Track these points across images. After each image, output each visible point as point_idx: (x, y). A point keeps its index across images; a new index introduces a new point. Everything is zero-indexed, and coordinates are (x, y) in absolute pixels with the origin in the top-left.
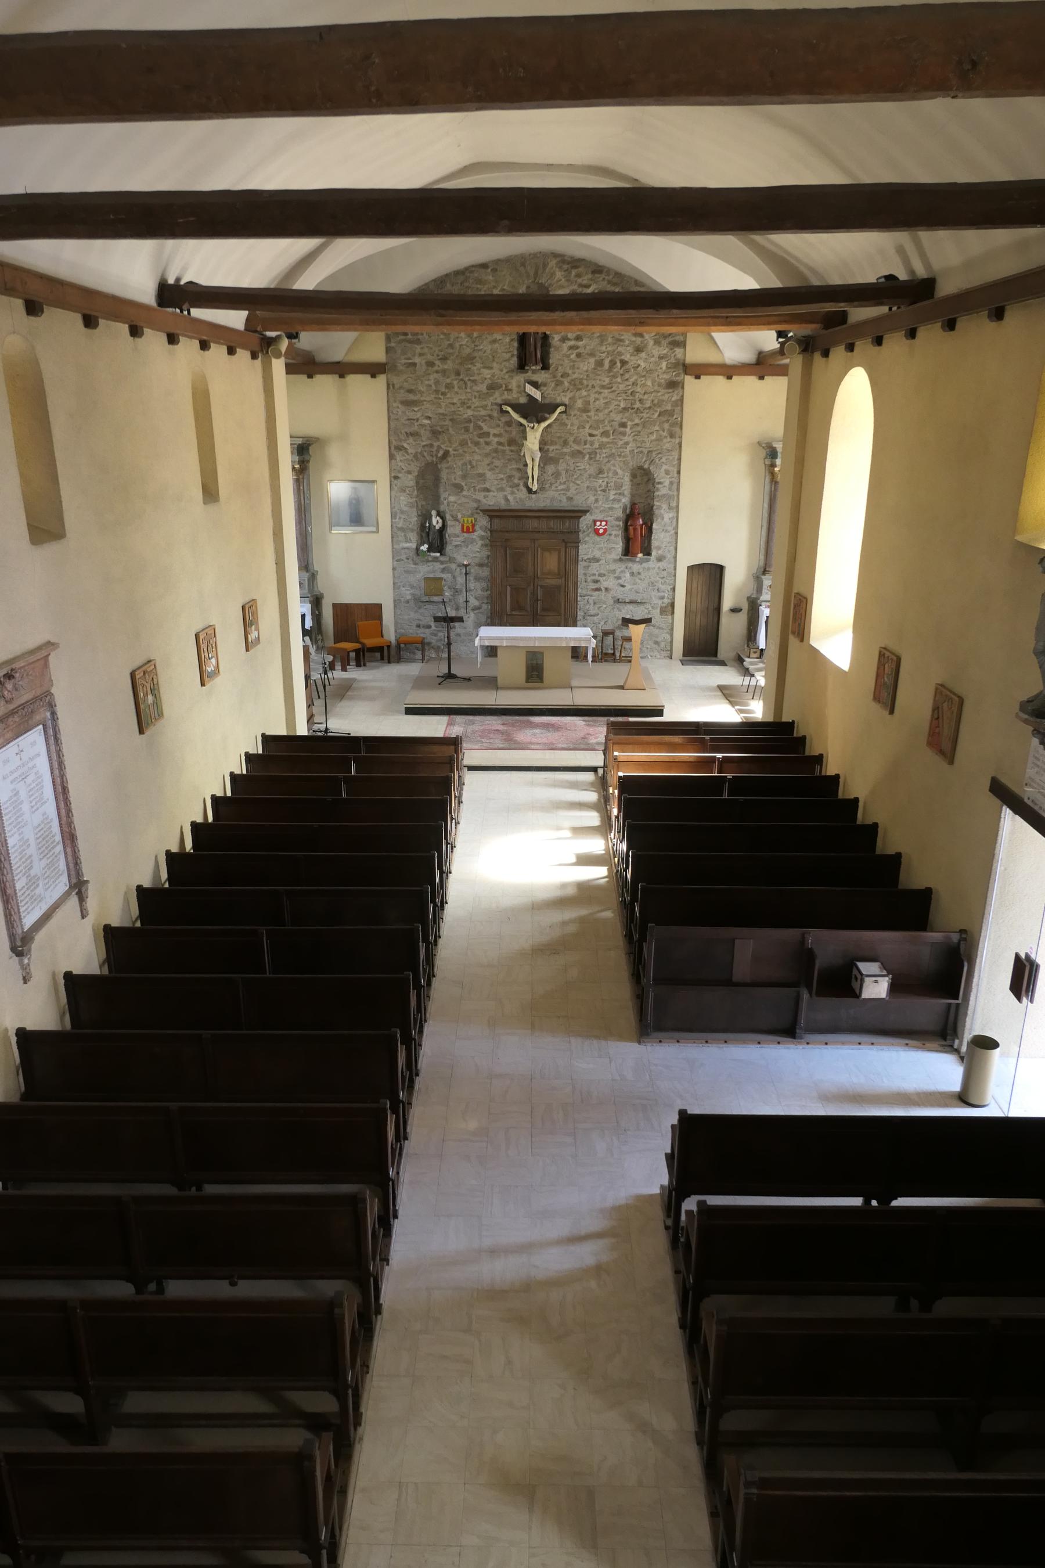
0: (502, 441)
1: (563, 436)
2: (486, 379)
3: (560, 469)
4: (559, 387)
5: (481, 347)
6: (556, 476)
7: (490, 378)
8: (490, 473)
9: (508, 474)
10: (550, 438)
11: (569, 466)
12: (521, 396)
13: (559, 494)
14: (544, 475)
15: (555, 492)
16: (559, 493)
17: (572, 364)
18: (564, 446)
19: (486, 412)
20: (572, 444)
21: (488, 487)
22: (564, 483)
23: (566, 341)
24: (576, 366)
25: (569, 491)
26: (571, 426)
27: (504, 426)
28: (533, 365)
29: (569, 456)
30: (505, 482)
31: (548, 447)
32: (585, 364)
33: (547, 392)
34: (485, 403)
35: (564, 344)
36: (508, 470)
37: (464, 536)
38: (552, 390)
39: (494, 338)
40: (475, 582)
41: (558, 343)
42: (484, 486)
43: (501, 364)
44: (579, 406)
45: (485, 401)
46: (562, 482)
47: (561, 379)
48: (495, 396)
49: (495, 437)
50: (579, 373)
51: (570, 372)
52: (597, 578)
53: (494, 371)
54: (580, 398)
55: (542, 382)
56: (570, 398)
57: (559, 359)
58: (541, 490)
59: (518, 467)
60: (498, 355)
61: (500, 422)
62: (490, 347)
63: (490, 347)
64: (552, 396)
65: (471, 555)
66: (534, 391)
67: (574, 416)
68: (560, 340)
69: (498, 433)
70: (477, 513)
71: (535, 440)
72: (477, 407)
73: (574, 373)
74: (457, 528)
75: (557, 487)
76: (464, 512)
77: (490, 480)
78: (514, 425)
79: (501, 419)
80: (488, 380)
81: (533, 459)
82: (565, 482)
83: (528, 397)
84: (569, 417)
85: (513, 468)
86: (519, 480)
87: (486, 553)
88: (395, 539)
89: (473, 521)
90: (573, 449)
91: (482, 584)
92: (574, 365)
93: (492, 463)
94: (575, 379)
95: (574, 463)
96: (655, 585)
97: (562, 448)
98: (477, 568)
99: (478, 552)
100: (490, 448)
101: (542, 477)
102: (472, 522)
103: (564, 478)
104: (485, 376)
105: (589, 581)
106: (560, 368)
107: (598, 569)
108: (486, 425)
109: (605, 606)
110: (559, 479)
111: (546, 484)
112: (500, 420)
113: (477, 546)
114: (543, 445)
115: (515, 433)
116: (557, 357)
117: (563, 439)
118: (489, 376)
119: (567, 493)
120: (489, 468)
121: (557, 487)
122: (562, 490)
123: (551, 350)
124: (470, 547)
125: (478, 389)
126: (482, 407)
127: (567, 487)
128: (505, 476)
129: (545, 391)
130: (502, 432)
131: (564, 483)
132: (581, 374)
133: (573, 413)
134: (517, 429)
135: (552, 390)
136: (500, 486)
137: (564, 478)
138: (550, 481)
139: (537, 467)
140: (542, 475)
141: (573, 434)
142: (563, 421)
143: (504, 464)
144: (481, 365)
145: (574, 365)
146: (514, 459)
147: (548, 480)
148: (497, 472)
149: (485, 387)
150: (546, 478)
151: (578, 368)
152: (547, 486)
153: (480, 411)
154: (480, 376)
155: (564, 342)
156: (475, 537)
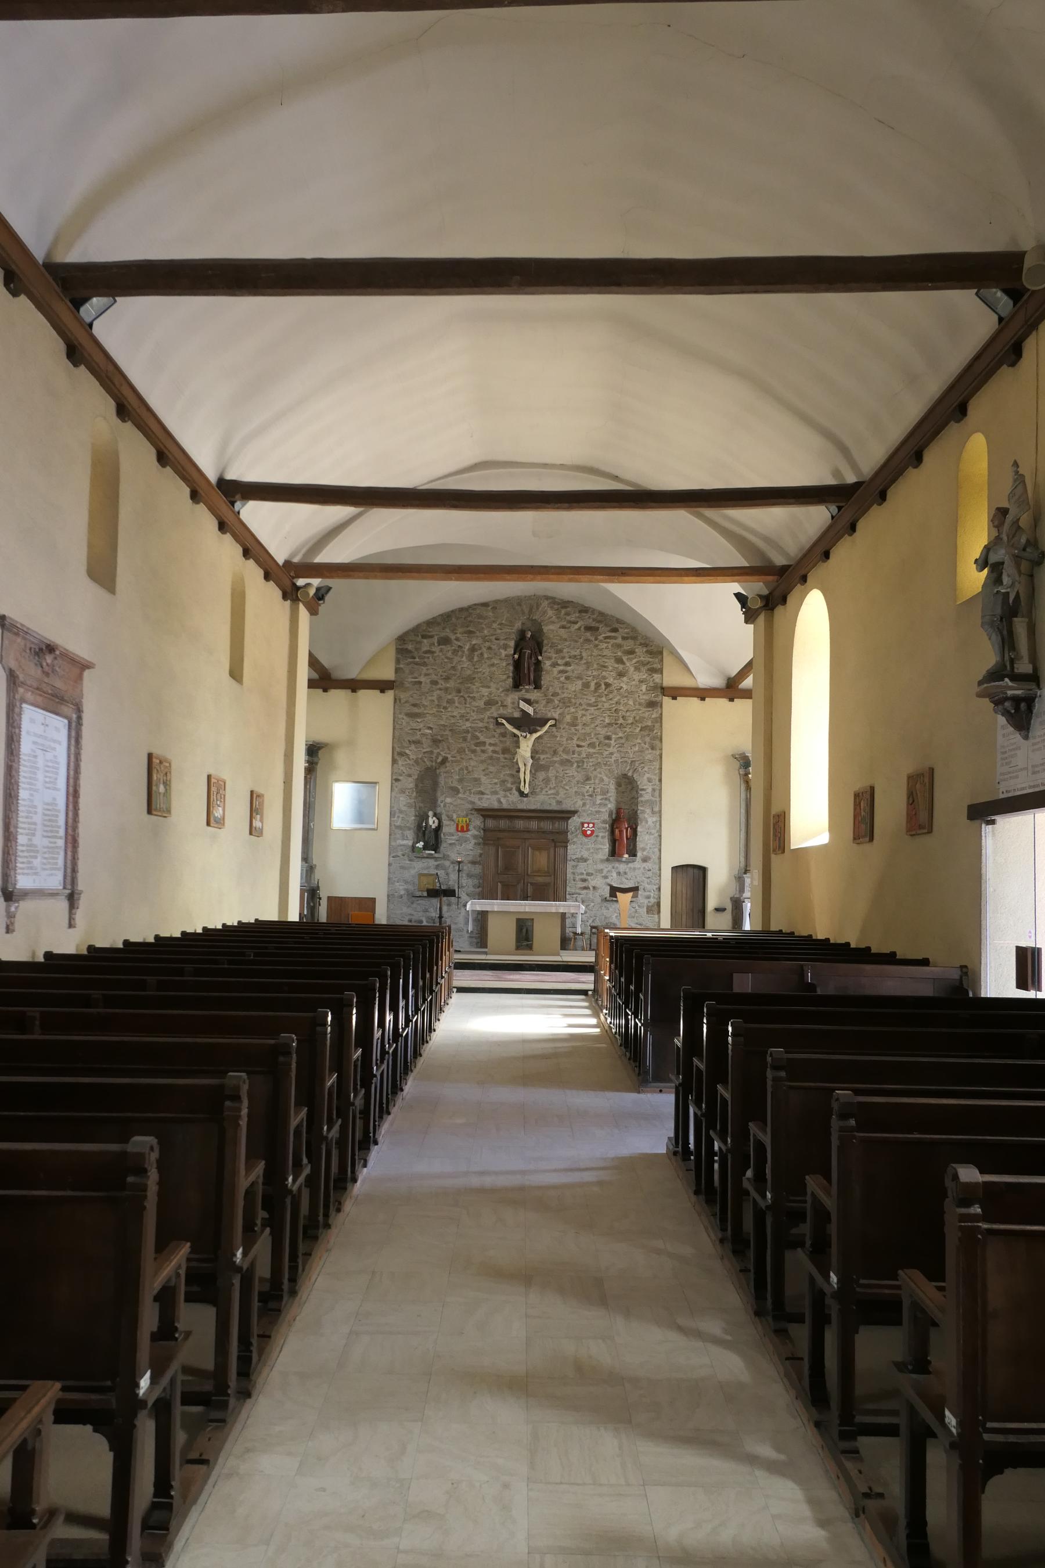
2: (483, 696)
3: (550, 775)
5: (481, 670)
7: (487, 696)
8: (485, 778)
15: (545, 796)
16: (549, 797)
18: (553, 755)
22: (554, 788)
23: (557, 666)
24: (565, 687)
25: (558, 795)
27: (499, 737)
30: (499, 786)
36: (502, 776)
37: (458, 835)
38: (543, 707)
40: (467, 879)
42: (479, 789)
43: (498, 683)
46: (552, 787)
47: (552, 698)
51: (560, 692)
52: (584, 877)
54: (568, 714)
56: (560, 714)
57: (549, 681)
60: (496, 676)
62: (488, 670)
63: (488, 670)
65: (464, 853)
67: (564, 729)
68: (551, 666)
70: (471, 814)
73: (563, 693)
74: (452, 827)
75: (547, 792)
76: (459, 813)
78: (508, 736)
81: (525, 765)
84: (559, 730)
87: (479, 851)
89: (468, 821)
91: (474, 881)
92: (563, 687)
93: (487, 769)
94: (564, 697)
98: (469, 865)
99: (471, 850)
102: (466, 822)
103: (554, 783)
105: (577, 879)
106: (551, 688)
107: (586, 868)
109: (592, 904)
112: (495, 732)
113: (470, 845)
117: (553, 749)
118: (487, 694)
120: (484, 773)
121: (547, 792)
122: (551, 794)
124: (463, 845)
125: (477, 704)
126: (479, 720)
129: (537, 708)
131: (554, 788)
132: (570, 694)
133: (562, 728)
135: (543, 707)
136: (493, 790)
137: (554, 783)
140: (533, 780)
141: (563, 745)
146: (507, 766)
151: (567, 689)
153: (477, 724)
155: (554, 667)
156: (468, 836)
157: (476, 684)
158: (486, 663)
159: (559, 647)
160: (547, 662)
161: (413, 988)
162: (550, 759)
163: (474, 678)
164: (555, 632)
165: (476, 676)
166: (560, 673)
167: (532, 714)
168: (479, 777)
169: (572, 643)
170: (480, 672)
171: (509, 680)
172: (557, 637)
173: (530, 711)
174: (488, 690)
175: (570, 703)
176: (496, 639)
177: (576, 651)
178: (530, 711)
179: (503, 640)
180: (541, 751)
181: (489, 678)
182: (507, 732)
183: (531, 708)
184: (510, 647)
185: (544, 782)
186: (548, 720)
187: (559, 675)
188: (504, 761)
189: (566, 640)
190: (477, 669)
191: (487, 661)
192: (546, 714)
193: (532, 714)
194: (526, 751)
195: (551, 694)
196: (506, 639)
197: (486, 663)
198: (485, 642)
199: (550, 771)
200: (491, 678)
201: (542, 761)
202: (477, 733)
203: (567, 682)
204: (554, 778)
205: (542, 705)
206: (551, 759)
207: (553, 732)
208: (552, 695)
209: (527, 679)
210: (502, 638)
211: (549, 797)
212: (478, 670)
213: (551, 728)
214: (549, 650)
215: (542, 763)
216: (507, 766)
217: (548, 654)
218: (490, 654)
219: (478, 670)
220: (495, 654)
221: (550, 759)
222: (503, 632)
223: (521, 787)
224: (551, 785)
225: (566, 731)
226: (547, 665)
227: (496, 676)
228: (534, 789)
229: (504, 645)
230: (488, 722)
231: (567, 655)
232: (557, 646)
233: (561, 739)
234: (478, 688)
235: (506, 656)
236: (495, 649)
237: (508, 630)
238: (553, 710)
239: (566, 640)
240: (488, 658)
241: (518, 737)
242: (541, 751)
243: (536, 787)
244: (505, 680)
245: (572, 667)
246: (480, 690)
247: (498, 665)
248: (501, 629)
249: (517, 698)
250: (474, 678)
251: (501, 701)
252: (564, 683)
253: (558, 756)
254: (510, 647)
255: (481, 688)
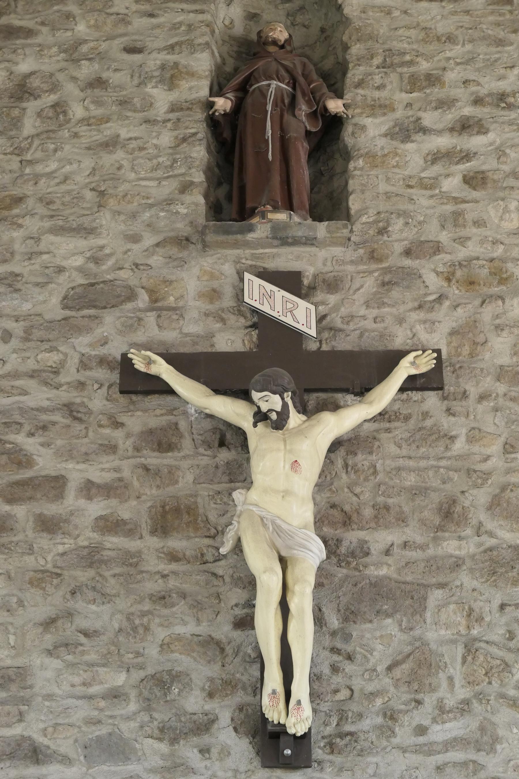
0: (125, 515)
1: (436, 483)
2: (60, 270)
3: (431, 636)
4: (395, 293)
5: (53, 166)
6: (413, 672)
7: (80, 270)
8: (55, 664)
9: (150, 671)
10: (366, 496)
11: (480, 619)
12: (220, 330)
13: (439, 769)
14: (349, 667)
15: (414, 759)
16: (440, 759)
17: (449, 208)
18: (440, 528)
19: (52, 393)
20: (483, 516)
21: (40, 739)
23: (419, 137)
24: (470, 217)
25: (492, 750)
26: (470, 440)
27: (137, 449)
28: (276, 209)
29: (471, 570)
30: (133, 707)
31: (362, 534)
32: (506, 210)
33: (344, 311)
34: (53, 358)
35: (410, 146)
36: (153, 651)
38: (367, 304)
39: (108, 133)
41: (382, 142)
42: (17, 730)
43: (134, 216)
44: (499, 361)
45: (51, 350)
46: (450, 702)
47: (407, 262)
48: (100, 331)
49: (90, 498)
50: (483, 241)
51: (444, 237)
53: (100, 242)
54: (499, 328)
55: (315, 276)
56: (453, 333)
57: (388, 196)
58: (332, 748)
59: (203, 629)
60: (123, 188)
61: (118, 434)
62: (88, 163)
63: (88, 163)
64: (369, 324)
66: (273, 309)
67: (482, 398)
68: (389, 135)
69: (108, 477)
71: (296, 478)
72: (15, 375)
73: (462, 241)
77: (49, 697)
78: (187, 444)
79: (123, 418)
80: (75, 274)
81: (283, 561)
82: (467, 702)
83: (255, 334)
84: (457, 406)
85: (179, 638)
86: (211, 695)
88: (63, 322)
90: (492, 542)
92: (457, 215)
93: (70, 615)
94: (470, 260)
95: (502, 607)
96: (474, 368)
97: (435, 539)
100: (61, 549)
101: (338, 680)
103: (458, 681)
104: (58, 261)
106: (397, 225)
108: (46, 445)
110: (433, 689)
111: (360, 716)
112: (117, 425)
114: (333, 524)
115: (190, 478)
116: (383, 187)
117: (435, 498)
118: (78, 261)
119: (481, 757)
120: (49, 639)
121: (421, 730)
123: (352, 165)
125: (26, 307)
126: (32, 375)
127: (482, 729)
128: (137, 675)
129: (336, 308)
130: (126, 473)
132: (495, 242)
133: (473, 391)
134: (205, 461)
135: (367, 304)
136: (103, 731)
137: (458, 681)
138: (379, 702)
139: (309, 589)
140: (335, 669)
141: (488, 474)
142: (428, 423)
143: (129, 617)
144: (47, 224)
145: (457, 215)
146: (183, 596)
147: (373, 695)
148: (92, 657)
149: (55, 300)
150: (357, 683)
151: (479, 223)
152: (366, 724)
153: (25, 393)
154: (38, 261)
155: (407, 138)
157: (27, 221)
158: (76, 135)
159: (424, 66)
160: (368, 121)
161: (268, 140)
162: (423, 547)
163: (19, 200)
164: (397, 13)
165: (29, 189)
166: (434, 161)
167: (313, 332)
168: (19, 662)
169: (482, 49)
170: (50, 175)
171: (188, 198)
172: (413, 33)
173: (302, 318)
174: (82, 244)
175: (502, 281)
176: (131, 50)
177: (501, 78)
178: (302, 318)
179: (159, 50)
180: (368, 512)
181: (89, 195)
182: (183, 425)
183: (302, 304)
184: (192, 74)
185: (397, 672)
186: (400, 355)
187: (436, 169)
188: (164, 567)
189: (450, 39)
190: (30, 162)
191: (83, 129)
192: (354, 82)
193: (313, 332)
194: (286, 493)
195: (398, 248)
196: (171, 48)
197: (76, 135)
198: (76, 61)
199: (428, 615)
200: (102, 194)
201: (378, 565)
202: (20, 439)
203: (475, 194)
204: (460, 650)
205: (360, 297)
206: (431, 552)
207: (426, 415)
208: (408, 253)
209: (276, 179)
210: (160, 43)
211: (440, 759)
212: (39, 168)
213: (416, 396)
214: (377, 80)
215: (383, 571)
216: (183, 596)
217: (377, 94)
218: (98, 103)
219: (39, 168)
220: (123, 103)
221: (423, 547)
222: (158, 26)
223: (266, 701)
224: (443, 691)
225: (496, 410)
226: (372, 132)
227: (123, 188)
228: (342, 718)
229: (163, 67)
230: (81, 385)
231: (459, 92)
232: (411, 63)
233: (476, 449)
234: (38, 240)
235: (172, 110)
236: (121, 87)
237: (181, 18)
238: (414, 316)
239: (450, 39)
240: (86, 121)
241: (241, 433)
242: (368, 512)
243: (354, 707)
244: (169, 201)
245: (491, 136)
246: (43, 246)
247: (134, 144)
248: (151, 15)
249: (229, 269)
250: (19, 200)
251: (151, 292)
252: (456, 200)
253: (469, 531)
254: (192, 74)
255: (52, 238)
